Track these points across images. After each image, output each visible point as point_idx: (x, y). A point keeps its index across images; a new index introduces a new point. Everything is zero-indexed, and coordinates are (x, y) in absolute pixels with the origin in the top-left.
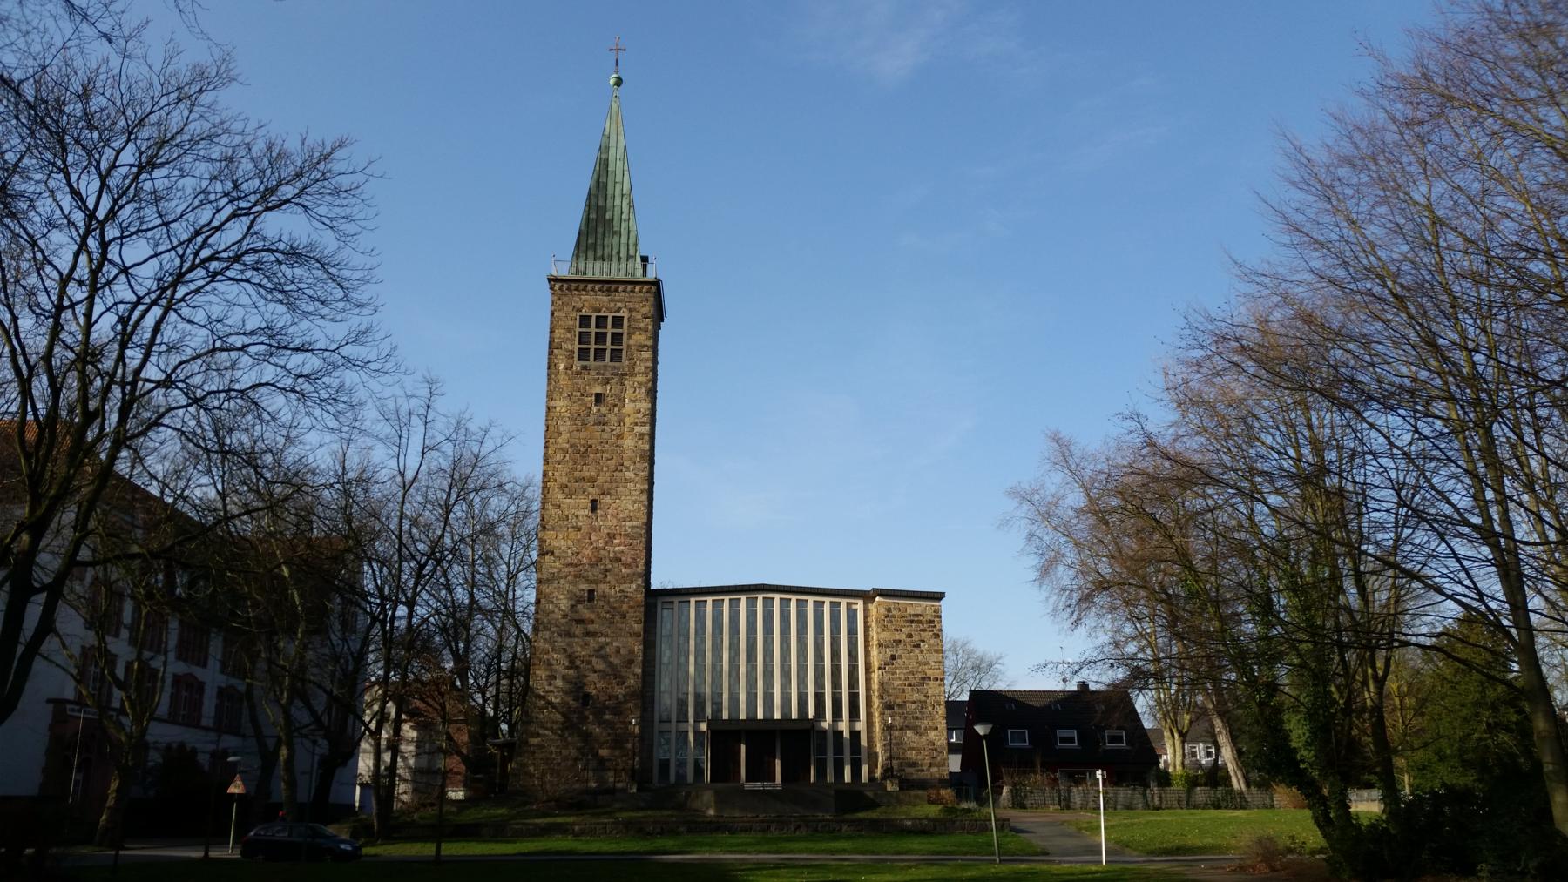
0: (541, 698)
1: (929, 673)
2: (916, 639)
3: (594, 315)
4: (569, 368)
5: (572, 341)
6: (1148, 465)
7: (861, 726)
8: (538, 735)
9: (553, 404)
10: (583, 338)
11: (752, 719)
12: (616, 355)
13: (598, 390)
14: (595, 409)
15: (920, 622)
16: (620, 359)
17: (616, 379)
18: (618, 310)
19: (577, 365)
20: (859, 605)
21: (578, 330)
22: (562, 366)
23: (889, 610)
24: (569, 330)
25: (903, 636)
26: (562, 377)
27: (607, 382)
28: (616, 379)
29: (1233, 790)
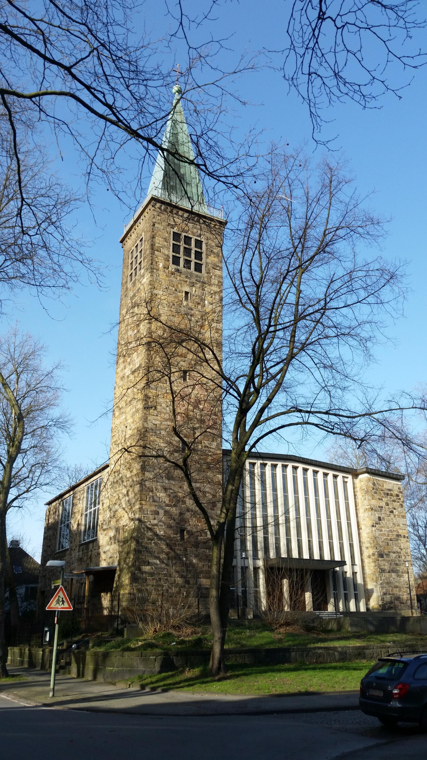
0: (150, 529)
1: (401, 532)
2: (391, 506)
3: (184, 234)
4: (166, 267)
5: (168, 248)
6: (54, 413)
7: (358, 569)
8: (149, 564)
9: (155, 292)
10: (176, 249)
11: (301, 559)
12: (198, 268)
13: (187, 289)
14: (185, 303)
15: (391, 495)
16: (200, 271)
17: (199, 285)
18: (200, 236)
19: (172, 268)
20: (350, 479)
21: (172, 242)
22: (161, 265)
23: (374, 484)
24: (166, 240)
25: (383, 504)
26: (161, 273)
27: (192, 285)
28: (199, 285)
29: (269, 557)
